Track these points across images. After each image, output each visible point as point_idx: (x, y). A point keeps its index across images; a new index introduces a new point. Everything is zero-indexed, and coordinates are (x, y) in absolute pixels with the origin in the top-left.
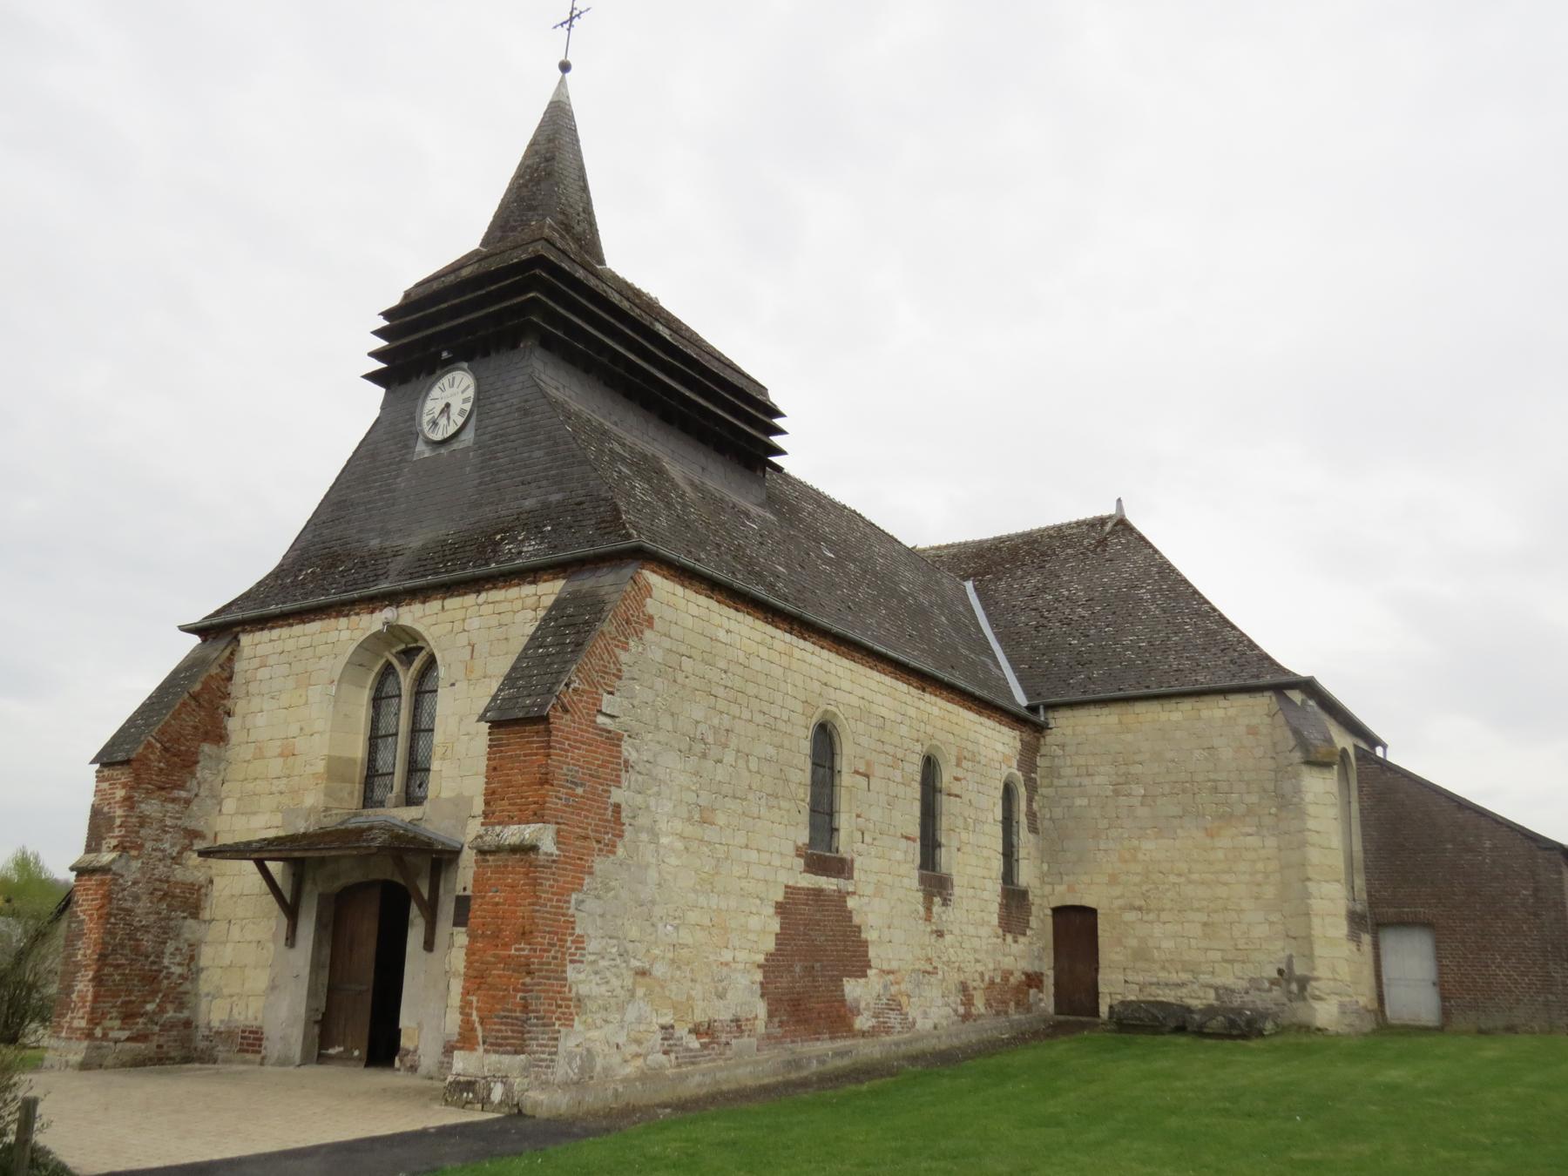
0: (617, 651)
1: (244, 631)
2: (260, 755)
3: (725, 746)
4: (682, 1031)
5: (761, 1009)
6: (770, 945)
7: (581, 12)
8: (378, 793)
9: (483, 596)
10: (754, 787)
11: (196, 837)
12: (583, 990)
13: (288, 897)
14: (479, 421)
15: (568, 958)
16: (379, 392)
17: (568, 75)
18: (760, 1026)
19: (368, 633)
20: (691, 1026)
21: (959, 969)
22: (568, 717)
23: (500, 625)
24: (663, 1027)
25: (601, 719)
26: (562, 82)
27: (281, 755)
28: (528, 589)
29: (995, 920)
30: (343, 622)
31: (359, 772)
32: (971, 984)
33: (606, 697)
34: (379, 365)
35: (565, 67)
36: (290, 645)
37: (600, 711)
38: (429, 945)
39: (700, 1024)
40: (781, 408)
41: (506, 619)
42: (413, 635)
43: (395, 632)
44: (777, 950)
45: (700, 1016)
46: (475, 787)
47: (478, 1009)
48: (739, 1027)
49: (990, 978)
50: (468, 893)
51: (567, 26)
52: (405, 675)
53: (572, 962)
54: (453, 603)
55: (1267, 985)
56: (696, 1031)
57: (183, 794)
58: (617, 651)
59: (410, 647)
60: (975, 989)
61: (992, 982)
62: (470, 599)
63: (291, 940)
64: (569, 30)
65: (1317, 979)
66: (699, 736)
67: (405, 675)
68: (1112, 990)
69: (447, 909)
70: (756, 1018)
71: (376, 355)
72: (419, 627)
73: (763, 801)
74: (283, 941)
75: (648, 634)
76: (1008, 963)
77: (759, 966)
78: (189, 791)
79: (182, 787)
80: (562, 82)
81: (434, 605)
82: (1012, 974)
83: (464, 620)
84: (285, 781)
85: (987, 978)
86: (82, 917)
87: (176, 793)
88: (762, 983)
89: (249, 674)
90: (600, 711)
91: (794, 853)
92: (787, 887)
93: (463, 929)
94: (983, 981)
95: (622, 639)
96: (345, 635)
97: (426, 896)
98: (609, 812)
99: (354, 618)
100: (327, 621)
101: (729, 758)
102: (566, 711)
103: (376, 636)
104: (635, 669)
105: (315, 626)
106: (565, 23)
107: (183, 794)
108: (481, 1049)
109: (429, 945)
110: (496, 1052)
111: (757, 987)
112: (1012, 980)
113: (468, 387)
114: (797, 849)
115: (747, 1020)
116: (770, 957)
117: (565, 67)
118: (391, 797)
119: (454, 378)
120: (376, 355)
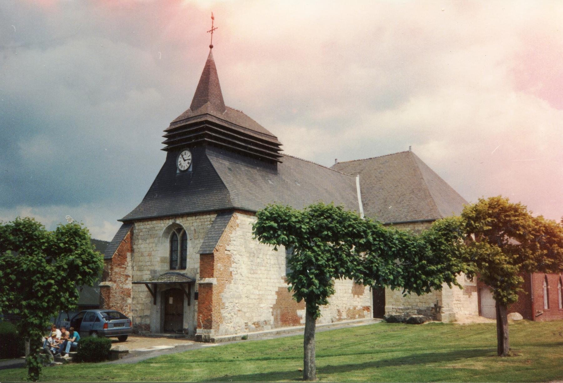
0: (229, 235)
1: (136, 222)
2: (142, 255)
3: (260, 253)
4: (249, 324)
5: (272, 318)
6: (274, 302)
7: (215, 29)
8: (174, 266)
9: (197, 217)
10: (268, 263)
11: (128, 277)
12: (224, 315)
13: (153, 292)
14: (193, 164)
15: (221, 308)
16: (165, 153)
17: (212, 49)
18: (272, 322)
19: (169, 225)
20: (253, 323)
21: (337, 306)
22: (218, 252)
23: (202, 225)
24: (246, 323)
25: (226, 252)
26: (210, 52)
27: (148, 255)
28: (208, 216)
29: (350, 291)
30: (162, 222)
31: (168, 260)
32: (341, 310)
33: (227, 246)
34: (166, 139)
35: (211, 47)
36: (148, 227)
37: (226, 250)
38: (189, 304)
39: (255, 322)
40: (282, 143)
41: (203, 223)
42: (179, 225)
43: (174, 224)
44: (276, 303)
45: (255, 320)
46: (197, 265)
47: (201, 319)
48: (266, 323)
49: (348, 308)
50: (197, 292)
51: (214, 28)
52: (179, 235)
53: (222, 309)
54: (189, 218)
55: (431, 309)
56: (254, 324)
57: (124, 266)
58: (229, 235)
59: (180, 228)
60: (343, 312)
61: (349, 309)
62: (194, 218)
63: (155, 303)
64: (212, 34)
65: (443, 307)
66: (252, 252)
67: (179, 235)
68: (389, 311)
69: (193, 296)
70: (271, 320)
71: (164, 143)
72: (181, 224)
73: (271, 266)
74: (153, 304)
75: (237, 229)
76: (355, 304)
77: (271, 308)
78: (125, 265)
79: (124, 264)
80: (210, 52)
81: (185, 219)
82: (357, 306)
83: (193, 223)
84: (149, 262)
85: (347, 309)
86: (103, 298)
87: (123, 266)
88: (272, 312)
89: (138, 234)
90: (226, 250)
91: (281, 278)
92: (279, 287)
93: (197, 301)
94: (346, 309)
95: (231, 231)
96: (163, 225)
97: (187, 292)
98: (229, 274)
99: (165, 221)
100: (157, 221)
101: (261, 256)
102: (217, 251)
103: (171, 226)
104: (234, 238)
105: (154, 222)
106: (211, 31)
107: (124, 266)
108: (203, 328)
109: (189, 304)
110: (206, 329)
111: (271, 313)
112: (357, 308)
113: (190, 156)
114: (282, 277)
115: (268, 321)
116: (274, 305)
117: (211, 47)
118: (177, 267)
119: (186, 153)
120: (164, 143)
